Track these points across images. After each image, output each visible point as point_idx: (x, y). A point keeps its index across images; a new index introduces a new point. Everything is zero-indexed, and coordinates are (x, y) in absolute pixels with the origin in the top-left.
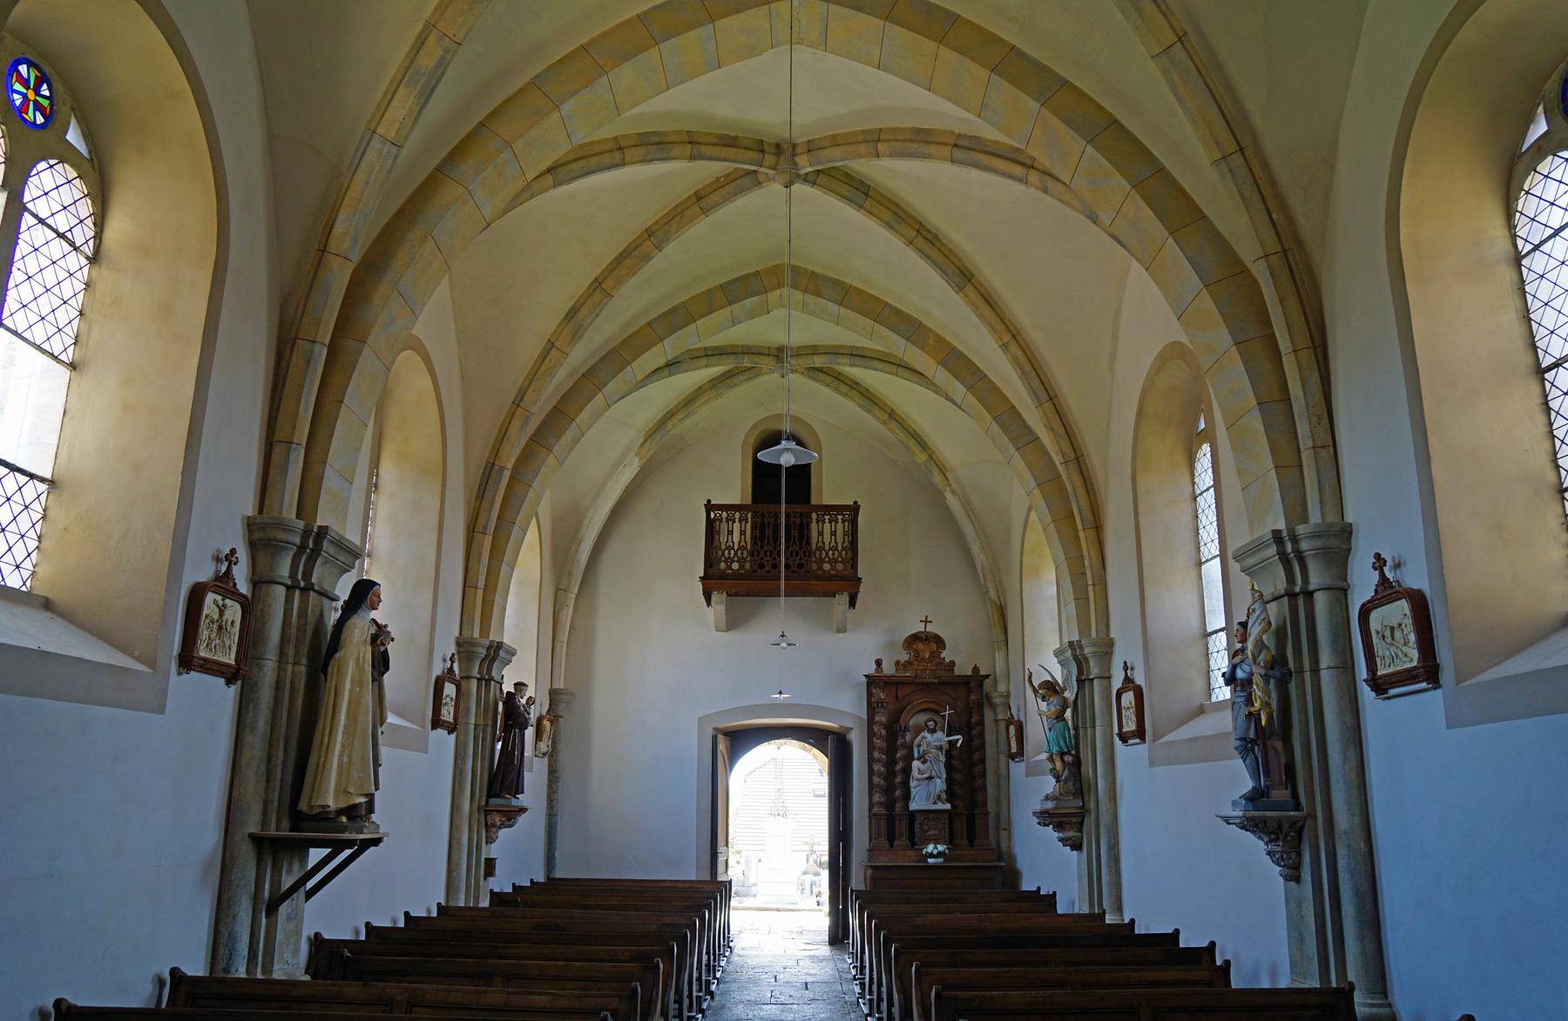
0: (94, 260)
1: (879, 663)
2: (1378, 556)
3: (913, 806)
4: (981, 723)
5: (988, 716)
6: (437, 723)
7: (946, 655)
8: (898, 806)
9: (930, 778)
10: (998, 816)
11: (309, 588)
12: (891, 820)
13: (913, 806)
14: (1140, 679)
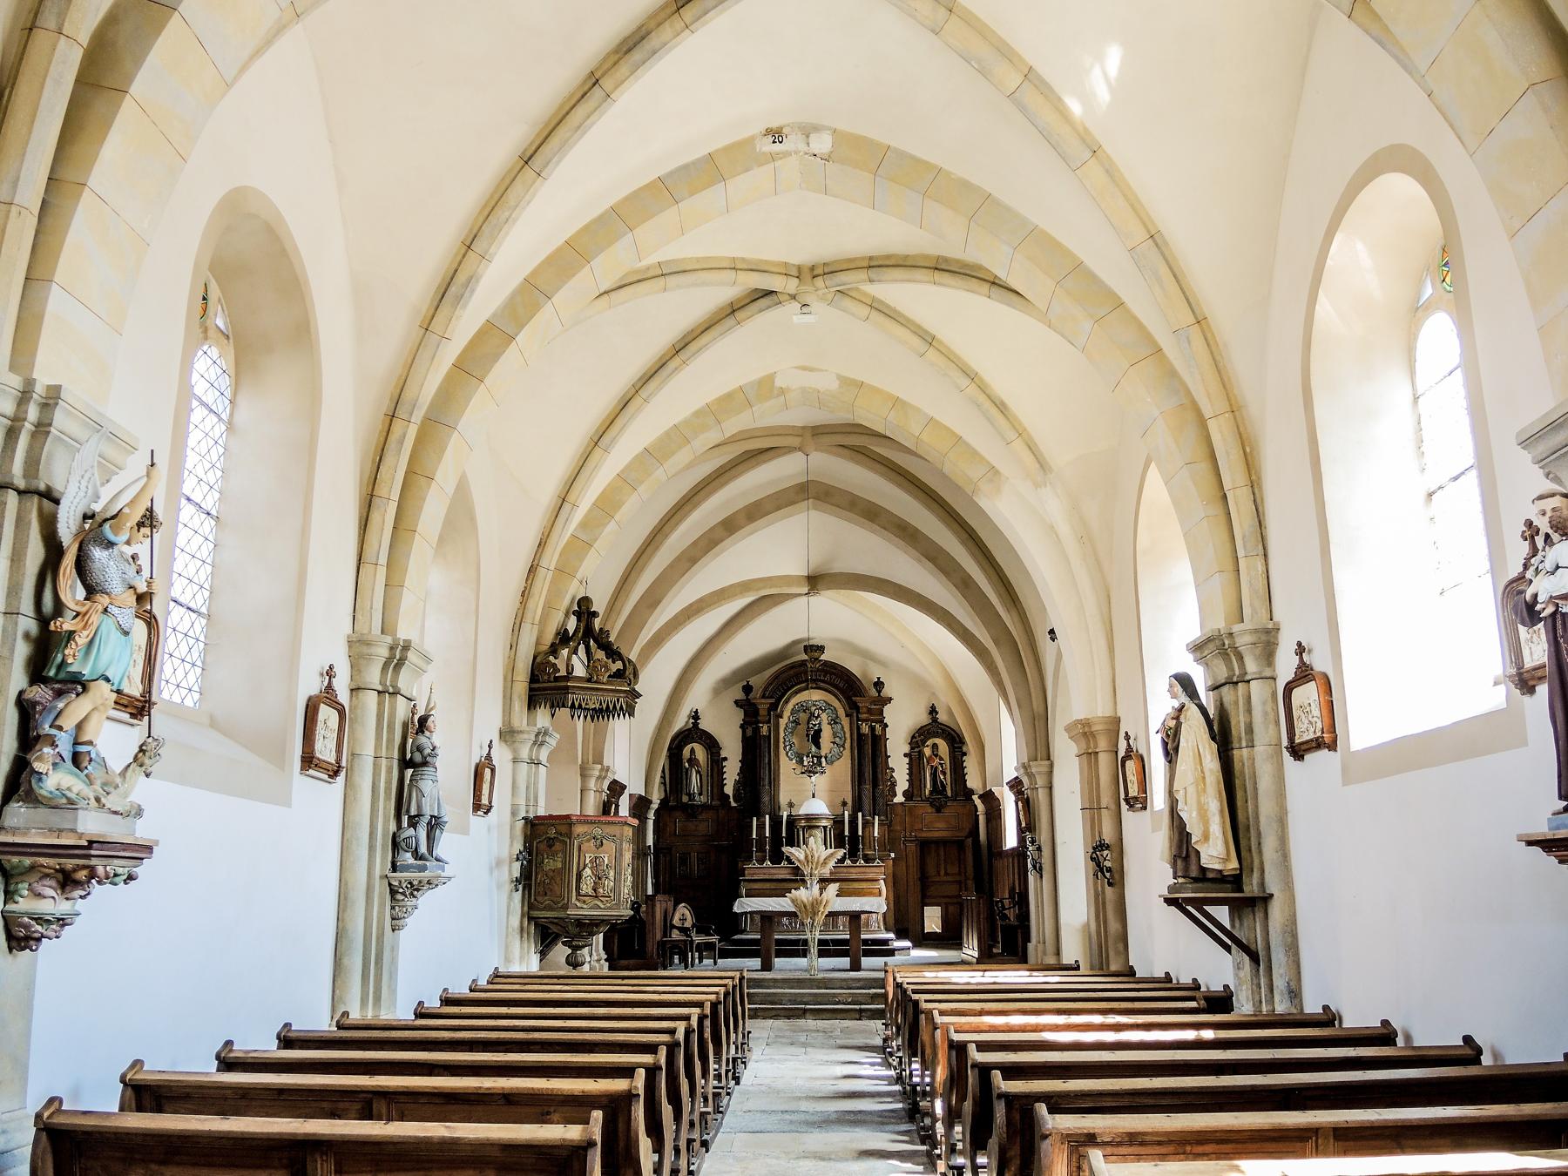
0: (230, 426)
2: (1299, 644)
6: (309, 760)
11: (396, 693)
14: (1319, 663)
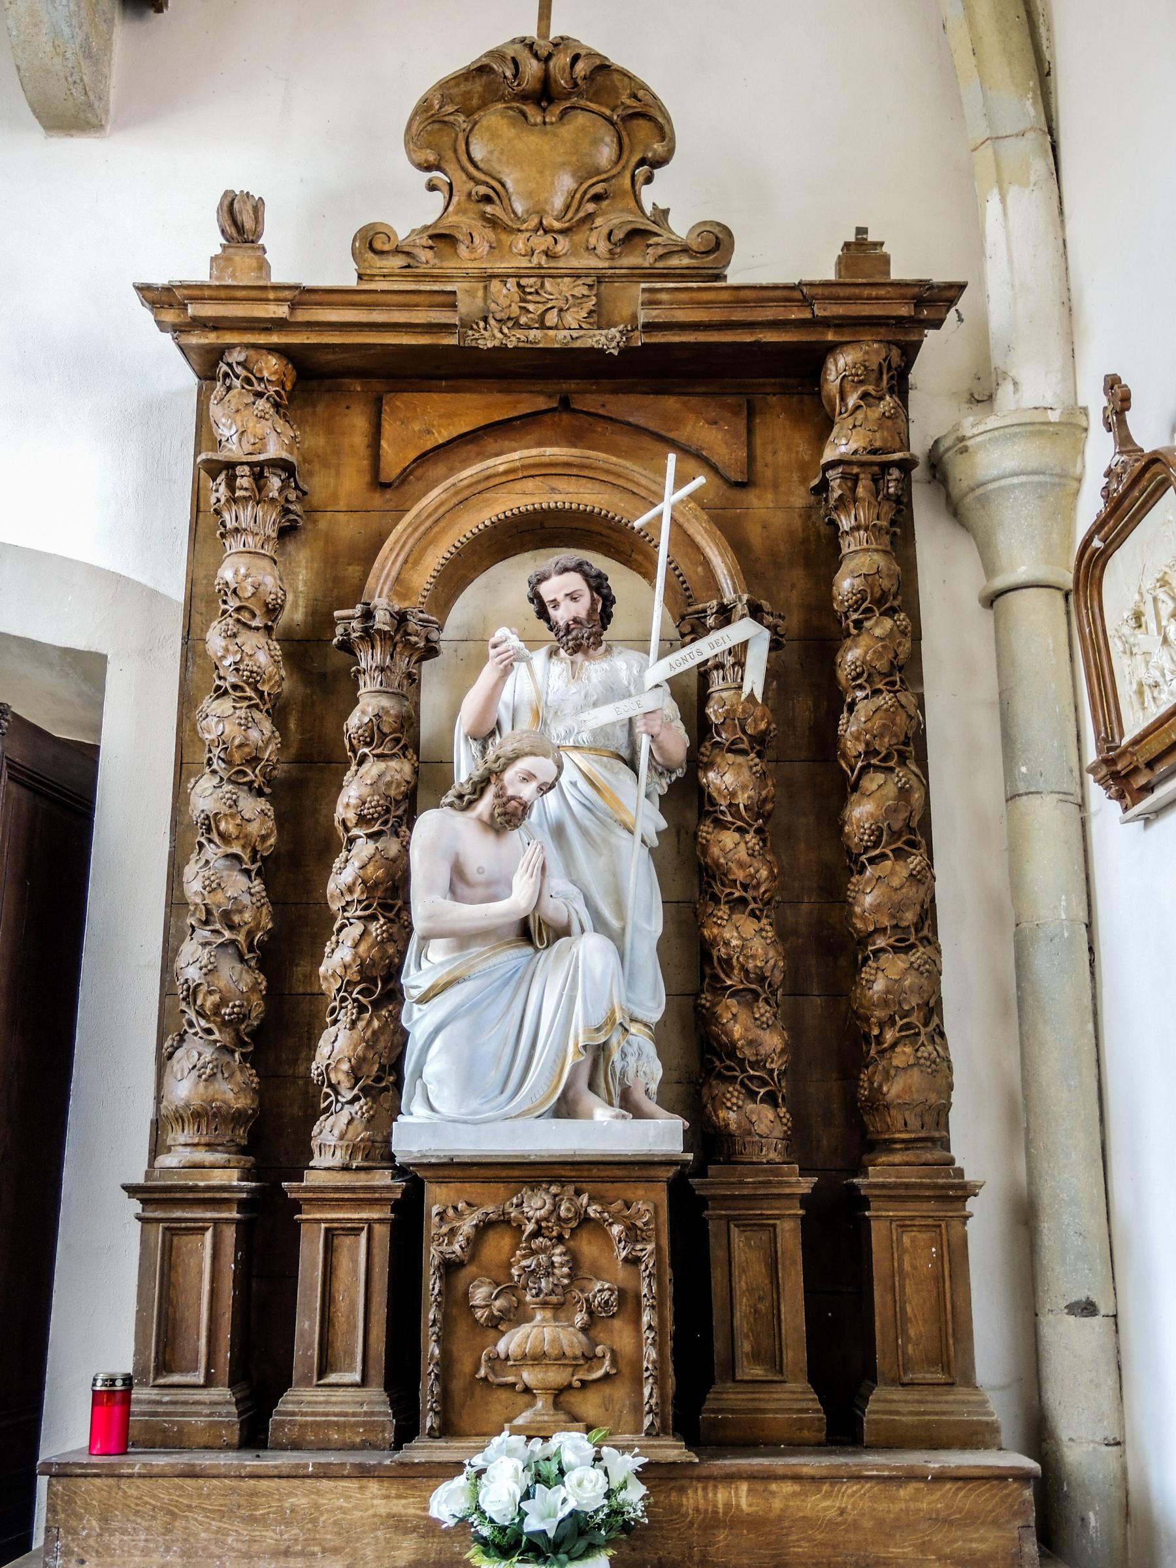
1: (240, 222)
3: (418, 1133)
4: (898, 597)
5: (944, 570)
7: (679, 198)
8: (332, 1136)
9: (533, 932)
10: (1025, 1216)
12: (267, 1236)
13: (418, 1133)
